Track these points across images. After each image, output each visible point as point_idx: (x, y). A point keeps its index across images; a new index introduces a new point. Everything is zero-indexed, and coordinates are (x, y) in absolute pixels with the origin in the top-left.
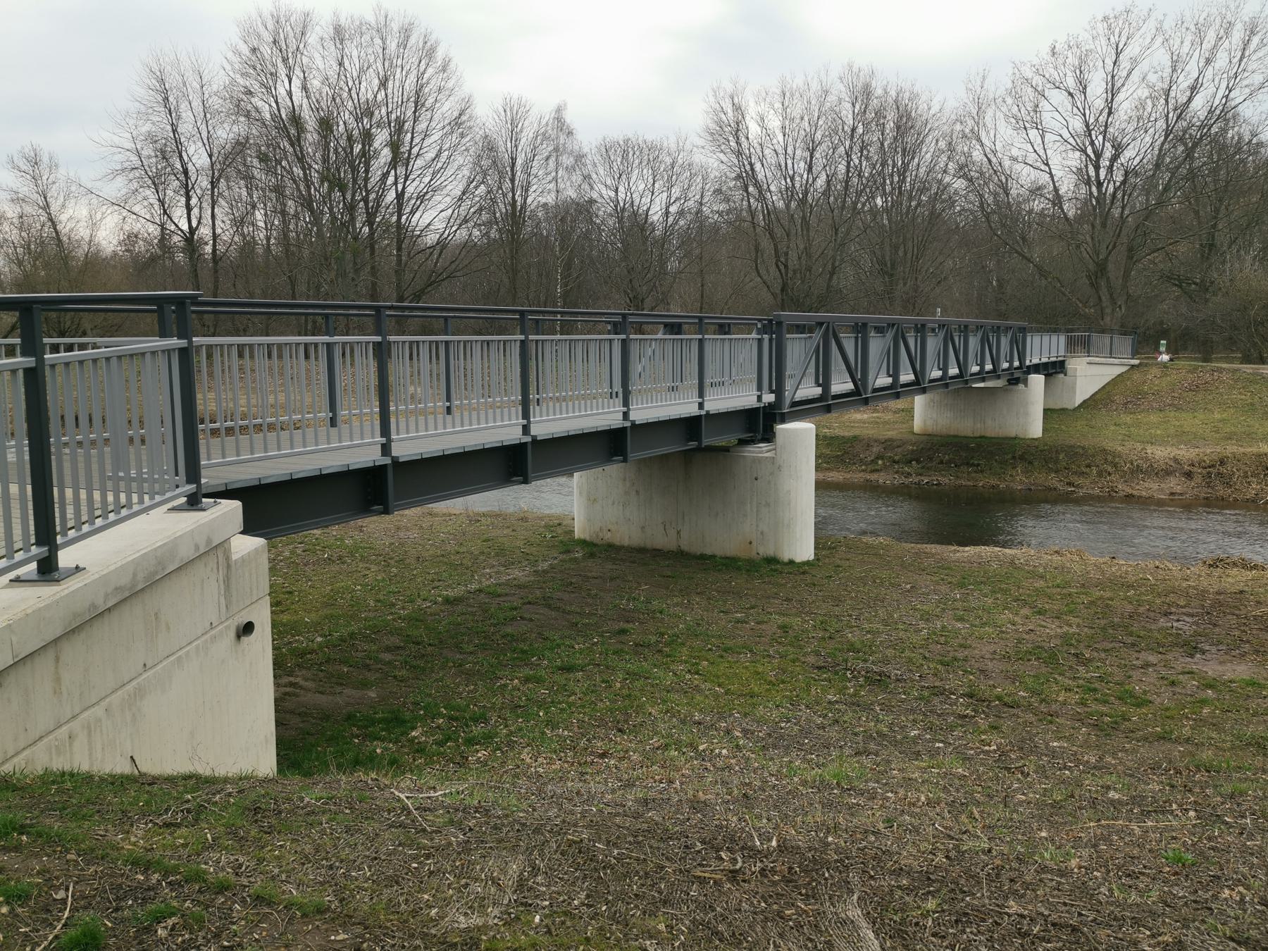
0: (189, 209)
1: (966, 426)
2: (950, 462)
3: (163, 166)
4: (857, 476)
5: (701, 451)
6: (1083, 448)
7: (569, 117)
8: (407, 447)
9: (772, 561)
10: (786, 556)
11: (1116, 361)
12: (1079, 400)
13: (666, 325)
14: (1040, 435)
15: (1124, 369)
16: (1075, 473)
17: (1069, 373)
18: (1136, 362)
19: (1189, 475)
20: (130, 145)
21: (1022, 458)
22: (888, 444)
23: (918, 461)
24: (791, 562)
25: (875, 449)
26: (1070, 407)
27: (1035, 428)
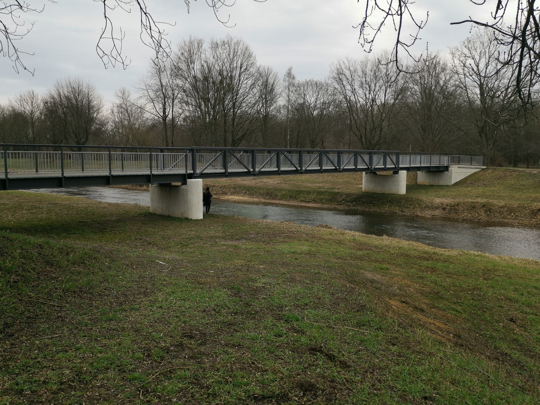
0: (385, 95)
1: (379, 189)
2: (365, 202)
3: (164, 95)
4: (333, 206)
5: (170, 187)
6: (412, 198)
7: (293, 72)
8: (12, 175)
9: (187, 219)
10: (190, 217)
11: (473, 167)
12: (453, 182)
13: (244, 151)
14: (405, 193)
15: (478, 170)
16: (405, 207)
17: (449, 170)
18: (485, 167)
19: (444, 209)
20: (145, 88)
21: (390, 201)
22: (348, 195)
23: (355, 202)
24: (191, 219)
25: (343, 197)
26: (450, 185)
27: (403, 191)
